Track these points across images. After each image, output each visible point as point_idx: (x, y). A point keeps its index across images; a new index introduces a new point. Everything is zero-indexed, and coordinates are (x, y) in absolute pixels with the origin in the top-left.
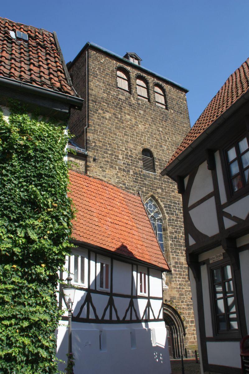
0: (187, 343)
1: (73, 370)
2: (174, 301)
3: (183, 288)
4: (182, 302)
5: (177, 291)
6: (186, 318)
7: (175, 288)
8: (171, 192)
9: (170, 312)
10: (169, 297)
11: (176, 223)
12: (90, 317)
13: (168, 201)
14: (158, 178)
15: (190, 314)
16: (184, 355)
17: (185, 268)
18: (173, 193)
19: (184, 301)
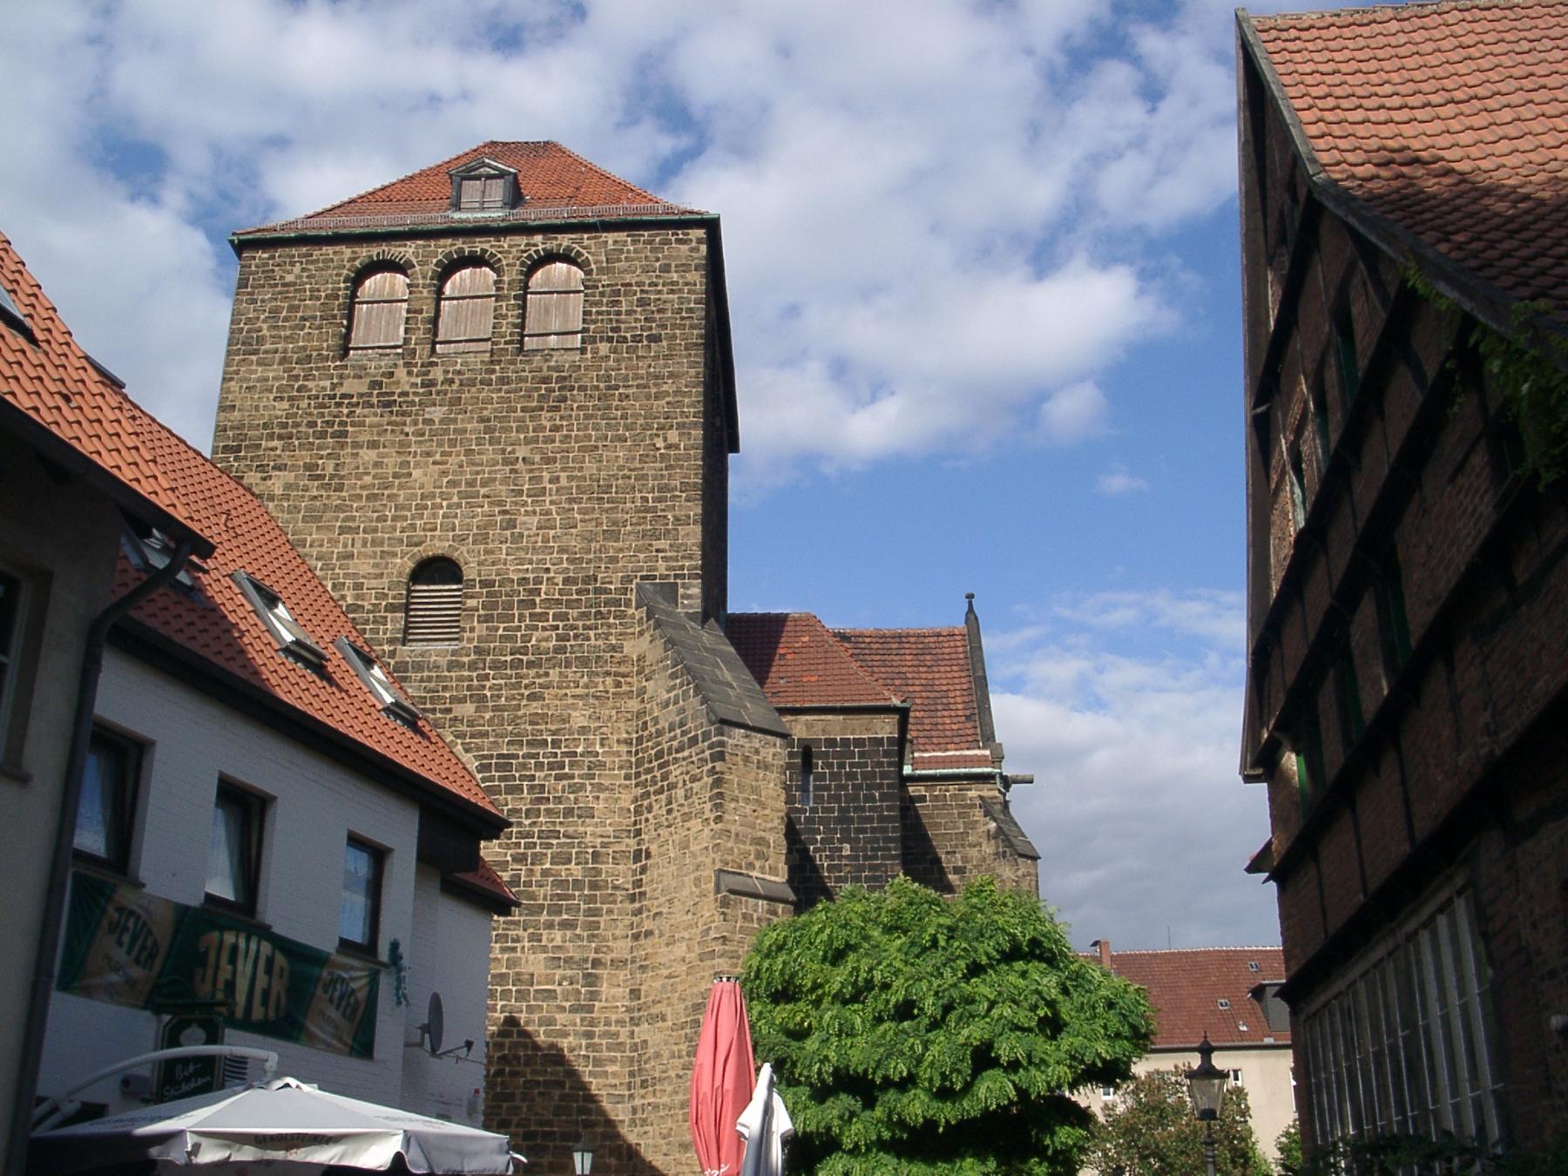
1: (546, 143)
3: (514, 1074)
8: (524, 702)
11: (527, 822)
12: (438, 346)
13: (500, 740)
14: (466, 659)
16: (281, 977)
17: (540, 996)
18: (535, 704)
19: (515, 1122)
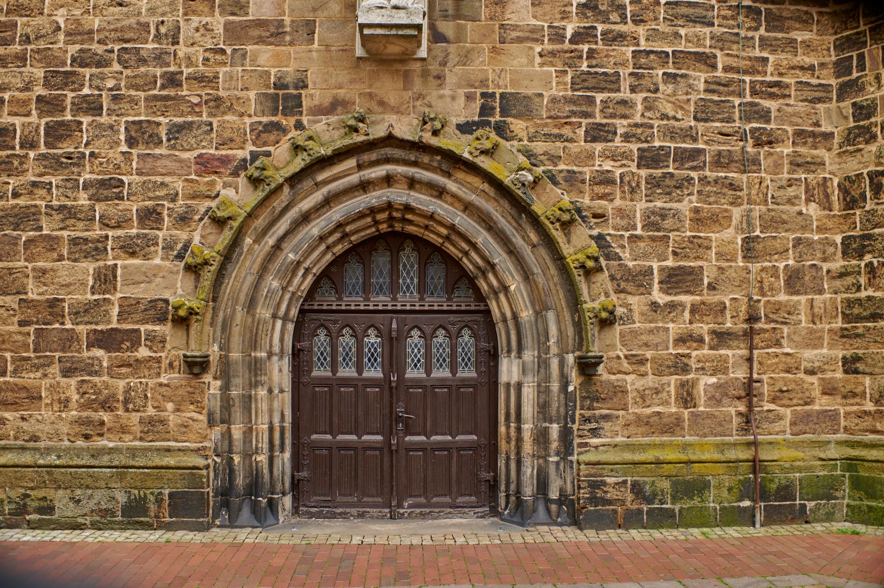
0: (607, 425)
2: (518, 126)
4: (597, 134)
5: (553, 54)
6: (626, 255)
7: (533, 35)
9: (468, 207)
10: (469, 97)
15: (668, 223)
